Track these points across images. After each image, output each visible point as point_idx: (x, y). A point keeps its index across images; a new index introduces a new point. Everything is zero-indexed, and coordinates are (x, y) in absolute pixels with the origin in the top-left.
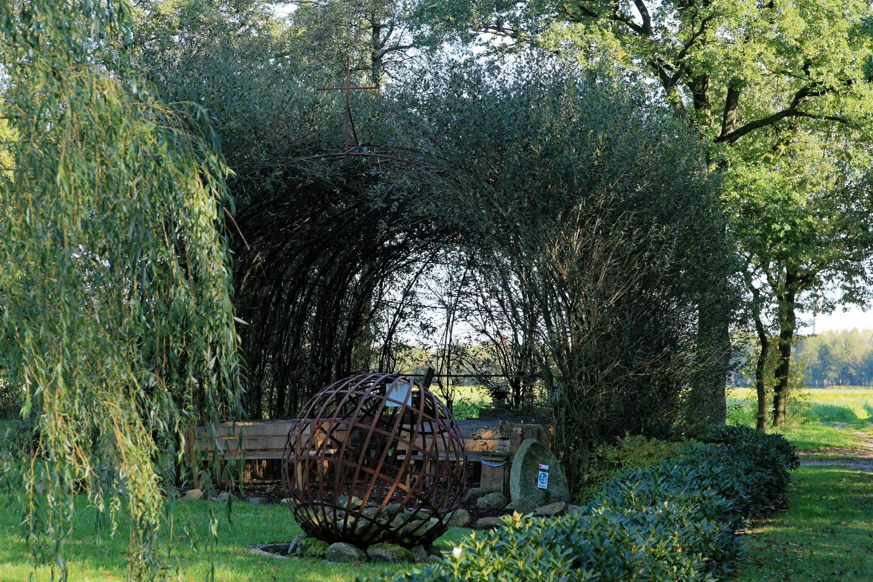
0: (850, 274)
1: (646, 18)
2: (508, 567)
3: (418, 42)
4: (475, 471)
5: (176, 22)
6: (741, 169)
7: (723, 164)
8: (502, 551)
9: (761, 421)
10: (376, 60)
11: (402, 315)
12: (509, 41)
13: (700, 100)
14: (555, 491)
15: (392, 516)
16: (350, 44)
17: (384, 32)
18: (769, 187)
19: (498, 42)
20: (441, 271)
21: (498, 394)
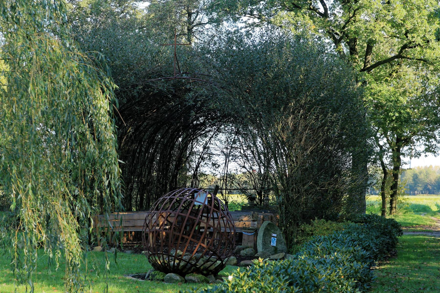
0: (429, 138)
1: (326, 9)
2: (256, 286)
3: (211, 21)
4: (239, 237)
5: (89, 11)
6: (374, 85)
7: (364, 83)
8: (253, 277)
9: (383, 212)
10: (190, 30)
11: (203, 159)
12: (257, 21)
13: (353, 51)
14: (280, 247)
15: (197, 260)
16: (176, 22)
17: (193, 16)
18: (387, 94)
19: (251, 21)
20: (222, 137)
21: (251, 198)
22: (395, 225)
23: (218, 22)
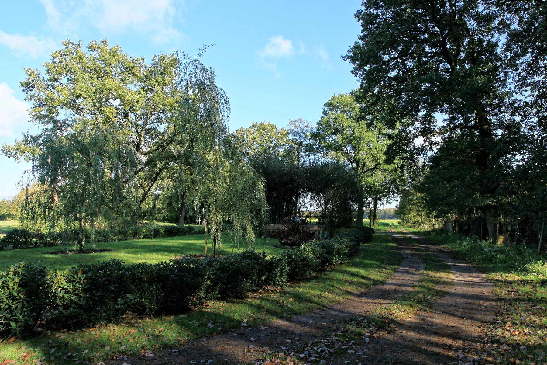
0: (387, 198)
1: (347, 151)
2: (311, 249)
3: (306, 155)
4: (314, 233)
5: (262, 152)
6: (366, 178)
7: (362, 178)
8: (311, 246)
9: (370, 225)
10: (298, 159)
11: (302, 205)
12: (323, 155)
13: (358, 166)
14: (328, 237)
15: (296, 241)
16: (293, 156)
17: (300, 154)
18: (371, 182)
19: (320, 155)
20: (309, 197)
21: (319, 220)
22: (372, 230)
23: (308, 156)
